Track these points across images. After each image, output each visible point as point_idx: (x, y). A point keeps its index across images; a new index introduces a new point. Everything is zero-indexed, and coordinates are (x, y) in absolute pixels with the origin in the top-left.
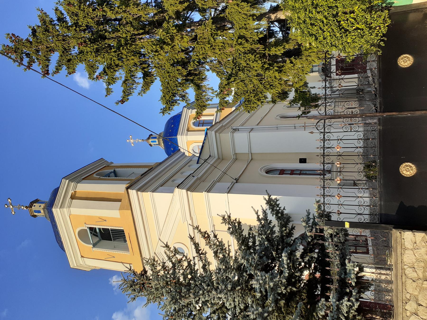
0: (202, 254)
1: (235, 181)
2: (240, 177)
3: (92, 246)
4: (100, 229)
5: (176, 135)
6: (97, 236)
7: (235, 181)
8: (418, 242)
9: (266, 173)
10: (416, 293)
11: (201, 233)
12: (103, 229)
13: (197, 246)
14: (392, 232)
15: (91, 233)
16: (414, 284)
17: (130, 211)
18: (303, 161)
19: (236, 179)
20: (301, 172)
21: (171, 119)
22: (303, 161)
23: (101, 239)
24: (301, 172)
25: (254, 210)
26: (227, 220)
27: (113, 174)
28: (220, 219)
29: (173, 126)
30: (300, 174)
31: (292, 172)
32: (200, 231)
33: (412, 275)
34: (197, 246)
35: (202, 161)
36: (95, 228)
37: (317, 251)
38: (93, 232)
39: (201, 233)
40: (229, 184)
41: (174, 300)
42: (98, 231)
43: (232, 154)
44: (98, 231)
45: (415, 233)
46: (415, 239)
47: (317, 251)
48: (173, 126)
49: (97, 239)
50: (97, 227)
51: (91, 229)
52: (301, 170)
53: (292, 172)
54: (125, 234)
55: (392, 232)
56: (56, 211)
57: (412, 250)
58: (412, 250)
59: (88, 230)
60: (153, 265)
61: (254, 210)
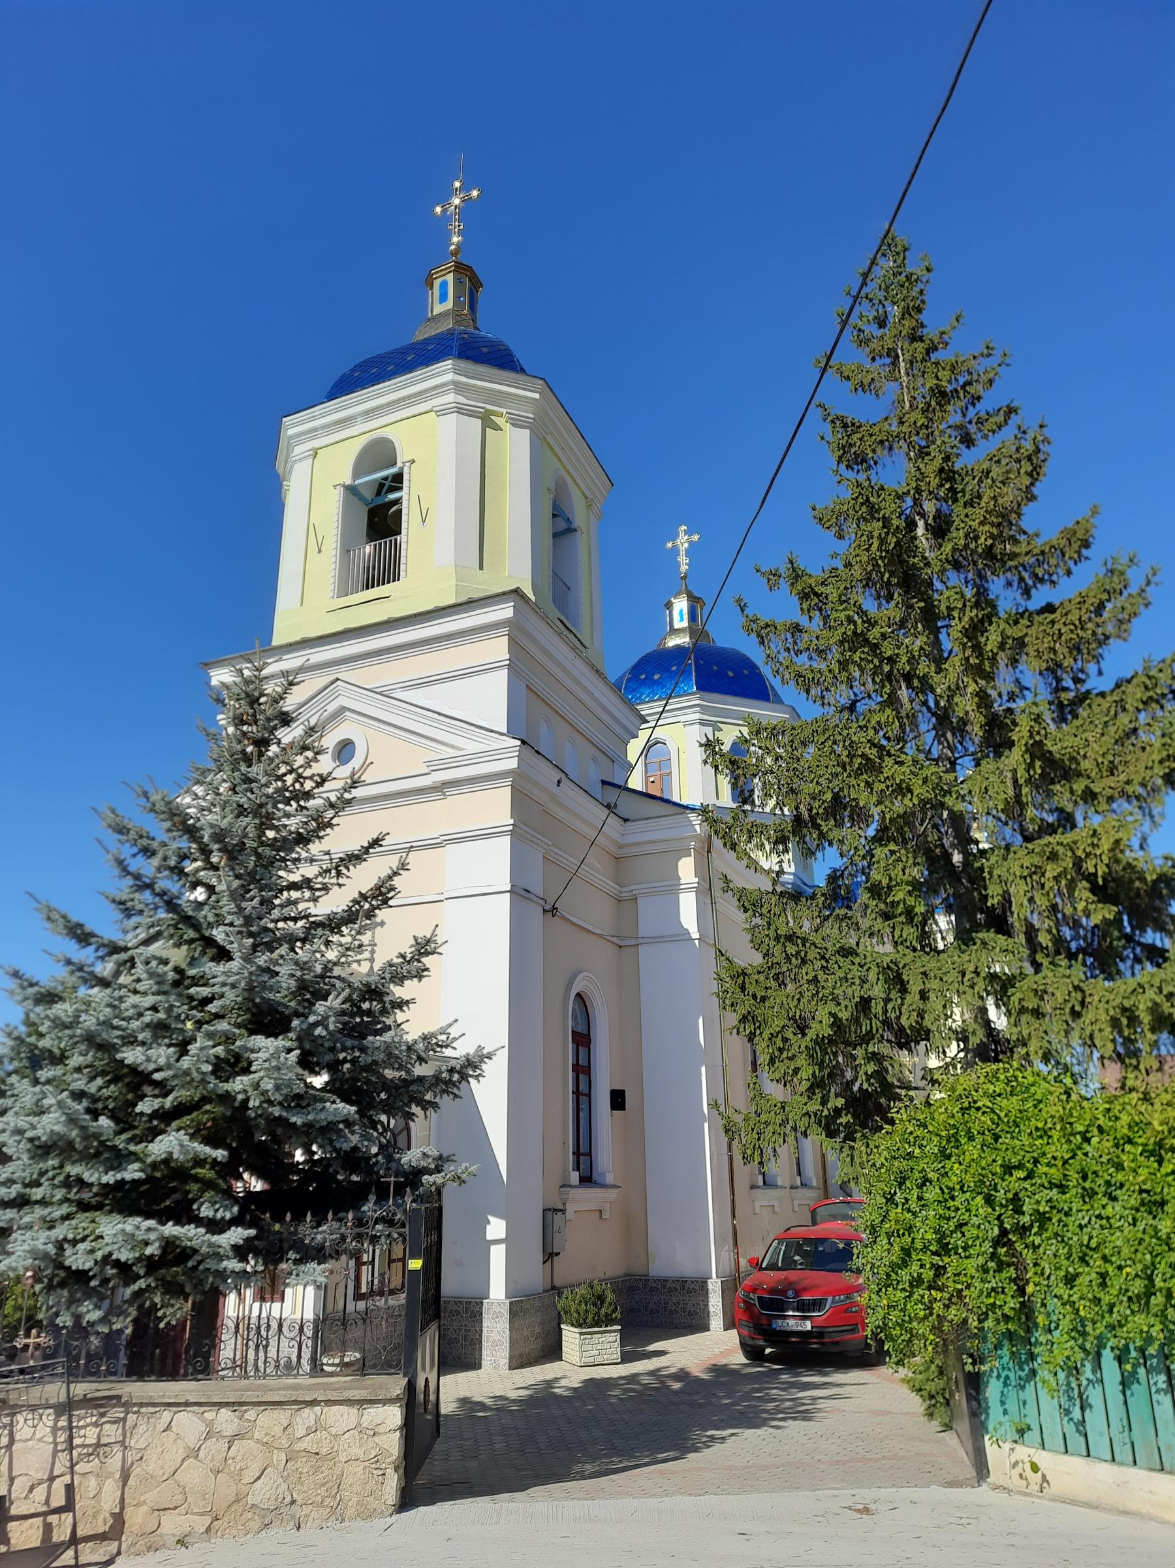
0: (339, 874)
1: (548, 907)
2: (563, 918)
3: (348, 482)
4: (398, 501)
5: (702, 687)
6: (379, 493)
7: (548, 907)
8: (376, 1439)
9: (578, 995)
10: (256, 1435)
11: (390, 878)
12: (400, 511)
13: (354, 858)
14: (401, 1376)
15: (386, 479)
16: (278, 1430)
17: (452, 601)
18: (618, 1100)
19: (554, 908)
20: (582, 1096)
21: (753, 667)
22: (618, 1100)
23: (371, 506)
24: (582, 1096)
25: (450, 1025)
26: (425, 948)
27: (562, 525)
28: (424, 932)
29: (731, 674)
30: (577, 1093)
31: (582, 1070)
32: (395, 874)
33: (300, 1427)
34: (354, 858)
35: (612, 795)
36: (401, 488)
37: (453, 247)
38: (388, 483)
39: (390, 878)
40: (537, 888)
41: (219, 836)
42: (393, 496)
43: (633, 887)
44: (393, 496)
45: (398, 1434)
46: (385, 1433)
47: (355, 1178)
48: (731, 674)
49: (369, 495)
50: (403, 494)
51: (398, 478)
52: (589, 1095)
53: (582, 1070)
54: (386, 586)
55: (401, 1376)
56: (445, 372)
57: (359, 1424)
58: (359, 1424)
59: (393, 470)
60: (305, 748)
61: (450, 1025)
